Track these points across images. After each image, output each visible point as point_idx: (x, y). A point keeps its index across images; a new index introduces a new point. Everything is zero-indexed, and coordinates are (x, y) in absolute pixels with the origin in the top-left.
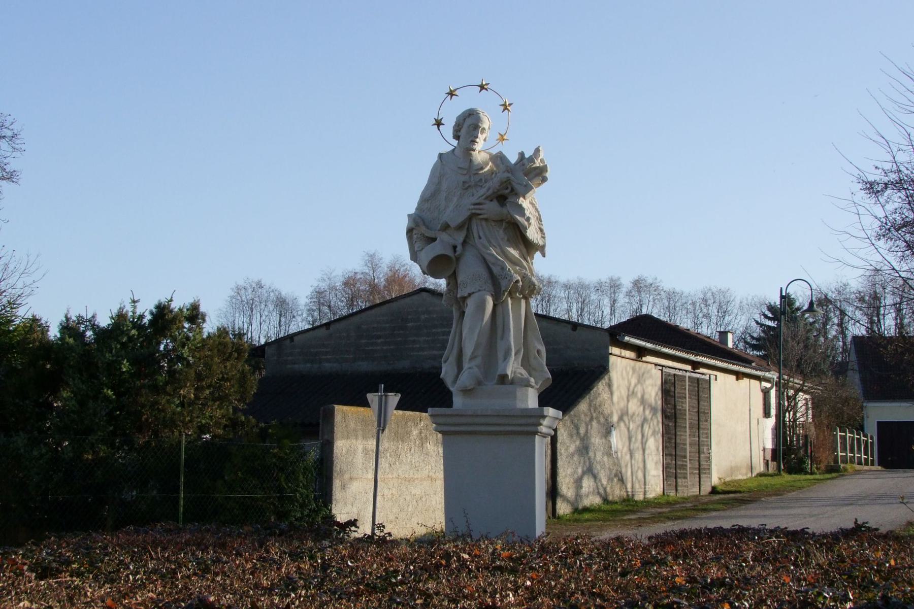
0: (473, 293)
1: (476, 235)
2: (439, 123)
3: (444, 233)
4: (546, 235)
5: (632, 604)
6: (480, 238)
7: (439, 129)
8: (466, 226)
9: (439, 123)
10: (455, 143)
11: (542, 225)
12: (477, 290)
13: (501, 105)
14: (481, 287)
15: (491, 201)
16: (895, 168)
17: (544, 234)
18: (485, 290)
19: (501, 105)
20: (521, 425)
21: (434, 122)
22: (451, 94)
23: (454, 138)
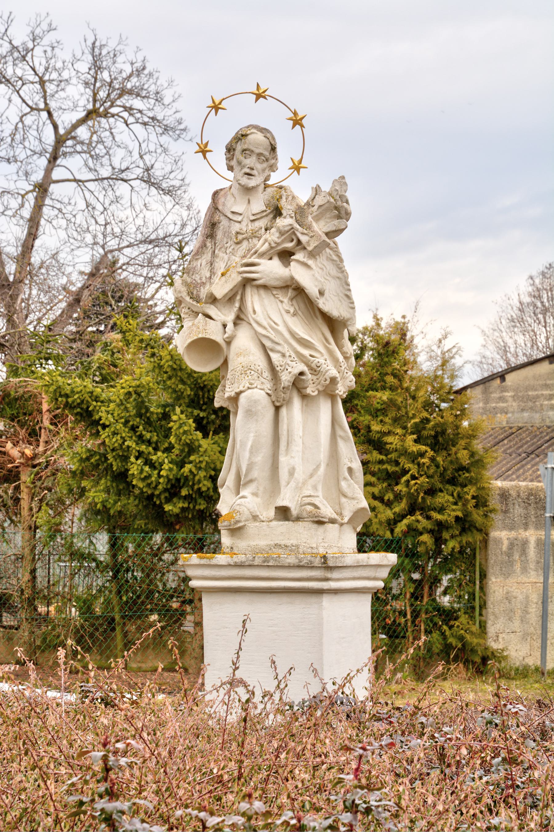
0: (241, 392)
1: (250, 309)
2: (204, 151)
3: (212, 306)
4: (356, 304)
5: (399, 831)
6: (254, 312)
7: (205, 157)
8: (238, 297)
9: (204, 151)
10: (230, 175)
11: (350, 290)
12: (246, 387)
13: (293, 128)
14: (251, 384)
15: (271, 259)
16: (29, 153)
17: (353, 303)
18: (256, 387)
19: (293, 128)
20: (354, 579)
21: (197, 148)
22: (216, 107)
23: (228, 170)
